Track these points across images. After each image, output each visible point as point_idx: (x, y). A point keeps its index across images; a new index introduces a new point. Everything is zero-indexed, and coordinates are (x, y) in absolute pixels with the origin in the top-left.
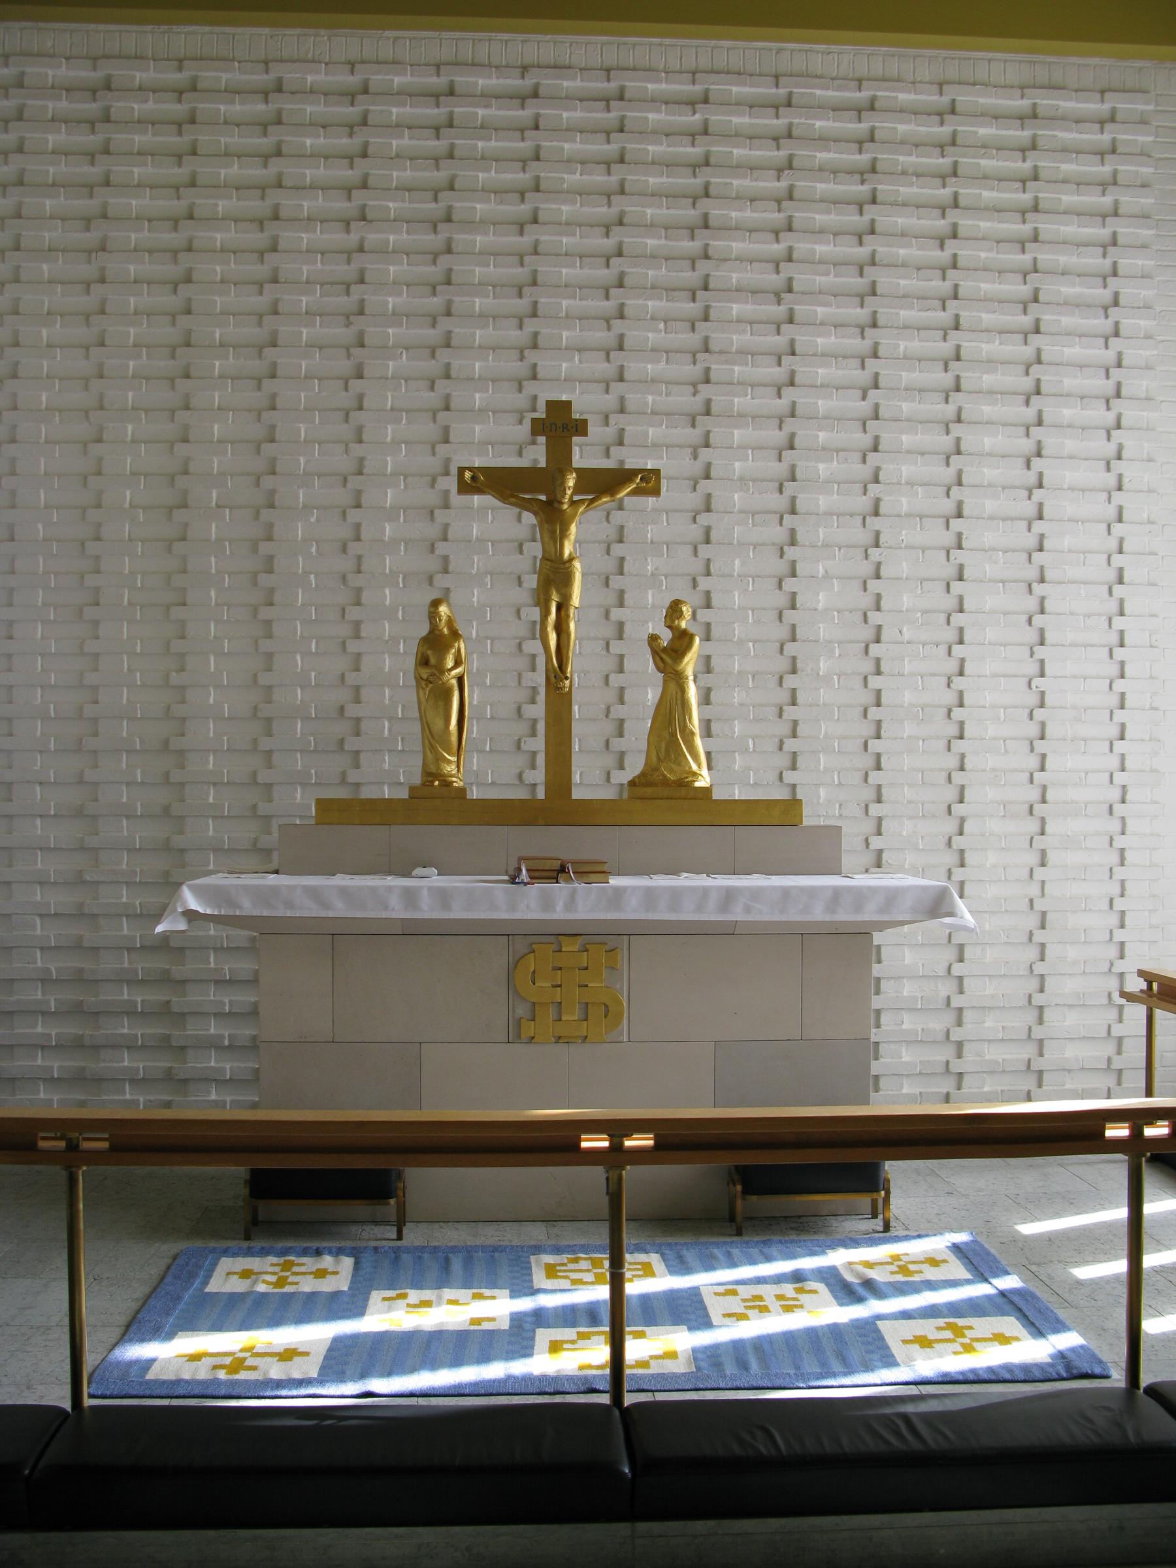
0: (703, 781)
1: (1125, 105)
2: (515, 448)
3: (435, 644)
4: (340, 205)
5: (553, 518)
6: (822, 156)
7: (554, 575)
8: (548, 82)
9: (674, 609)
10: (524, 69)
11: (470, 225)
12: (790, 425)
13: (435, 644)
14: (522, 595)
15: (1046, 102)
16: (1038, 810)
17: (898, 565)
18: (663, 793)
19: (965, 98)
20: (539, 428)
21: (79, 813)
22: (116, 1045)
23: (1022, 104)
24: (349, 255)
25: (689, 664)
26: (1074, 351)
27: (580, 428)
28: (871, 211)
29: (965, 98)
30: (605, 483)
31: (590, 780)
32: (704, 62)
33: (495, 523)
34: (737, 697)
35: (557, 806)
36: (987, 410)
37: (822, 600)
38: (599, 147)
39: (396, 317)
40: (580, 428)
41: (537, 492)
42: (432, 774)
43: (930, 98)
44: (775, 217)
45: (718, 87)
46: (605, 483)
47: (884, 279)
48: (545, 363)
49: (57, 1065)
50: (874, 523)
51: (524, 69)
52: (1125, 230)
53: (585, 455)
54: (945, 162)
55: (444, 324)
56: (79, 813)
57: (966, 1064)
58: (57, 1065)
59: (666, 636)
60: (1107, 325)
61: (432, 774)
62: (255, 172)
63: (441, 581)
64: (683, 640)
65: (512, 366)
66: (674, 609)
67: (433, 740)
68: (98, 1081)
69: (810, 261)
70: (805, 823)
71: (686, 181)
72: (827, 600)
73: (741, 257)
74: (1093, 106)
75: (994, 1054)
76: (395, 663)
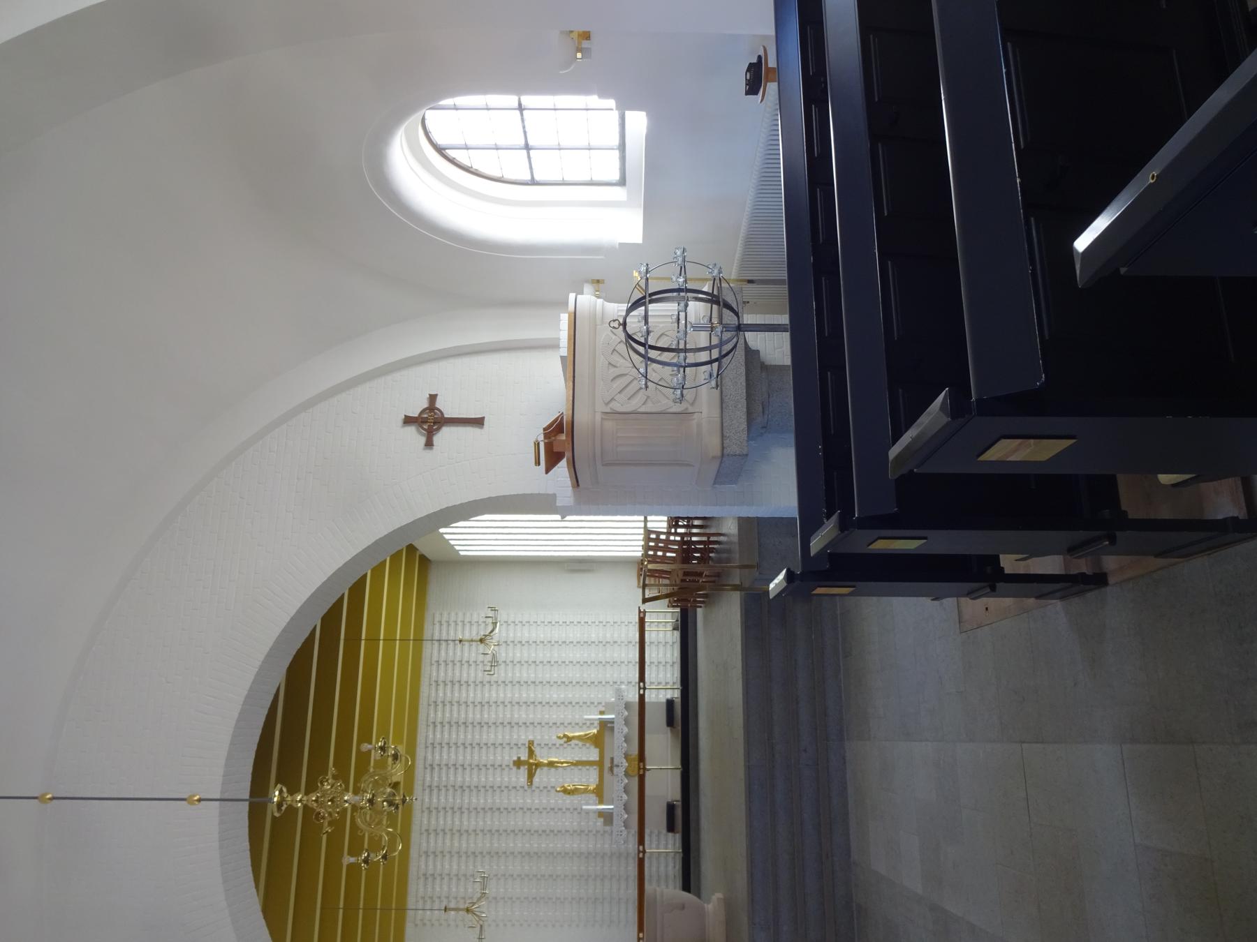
1: (437, 619)
2: (523, 771)
3: (566, 791)
4: (458, 814)
5: (539, 765)
7: (551, 764)
8: (429, 762)
13: (566, 791)
16: (604, 644)
18: (597, 741)
19: (435, 658)
22: (658, 871)
24: (470, 812)
30: (531, 753)
31: (593, 755)
33: (541, 777)
35: (600, 764)
38: (445, 749)
42: (593, 792)
45: (431, 720)
46: (531, 753)
48: (506, 763)
52: (467, 620)
53: (524, 757)
57: (663, 661)
65: (498, 770)
68: (667, 876)
70: (665, 518)
71: (454, 728)
72: (555, 695)
73: (473, 715)
74: (437, 626)
76: (568, 800)
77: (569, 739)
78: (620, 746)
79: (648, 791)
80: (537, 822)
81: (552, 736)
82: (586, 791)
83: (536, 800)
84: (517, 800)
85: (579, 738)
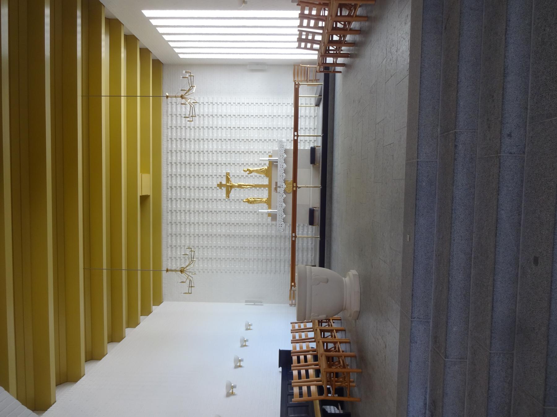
0: (266, 167)
3: (249, 202)
5: (232, 187)
6: (179, 146)
7: (240, 186)
8: (169, 185)
9: (244, 171)
10: (168, 188)
11: (190, 196)
12: (218, 152)
13: (249, 202)
14: (242, 189)
15: (169, 113)
17: (238, 137)
18: (268, 173)
20: (221, 188)
21: (271, 250)
23: (170, 117)
25: (251, 169)
26: (206, 109)
27: (221, 183)
28: (187, 139)
29: (169, 125)
30: (228, 180)
31: (266, 181)
32: (166, 163)
34: (256, 160)
35: (269, 186)
36: (215, 123)
37: (243, 123)
39: (203, 206)
40: (221, 183)
41: (229, 188)
42: (265, 202)
43: (169, 130)
44: (188, 153)
46: (228, 180)
47: (197, 138)
49: (305, 254)
50: (232, 140)
51: (168, 188)
53: (224, 182)
54: (179, 128)
55: (204, 200)
56: (271, 250)
58: (305, 254)
59: (248, 172)
60: (202, 104)
61: (265, 202)
62: (183, 226)
63: (240, 200)
64: (248, 170)
66: (244, 171)
67: (261, 202)
69: (194, 148)
75: (307, 124)
76: (251, 207)
77: (251, 172)
78: (282, 175)
79: (298, 202)
80: (233, 219)
81: (240, 171)
82: (261, 202)
83: (228, 206)
84: (221, 206)
85: (257, 171)
